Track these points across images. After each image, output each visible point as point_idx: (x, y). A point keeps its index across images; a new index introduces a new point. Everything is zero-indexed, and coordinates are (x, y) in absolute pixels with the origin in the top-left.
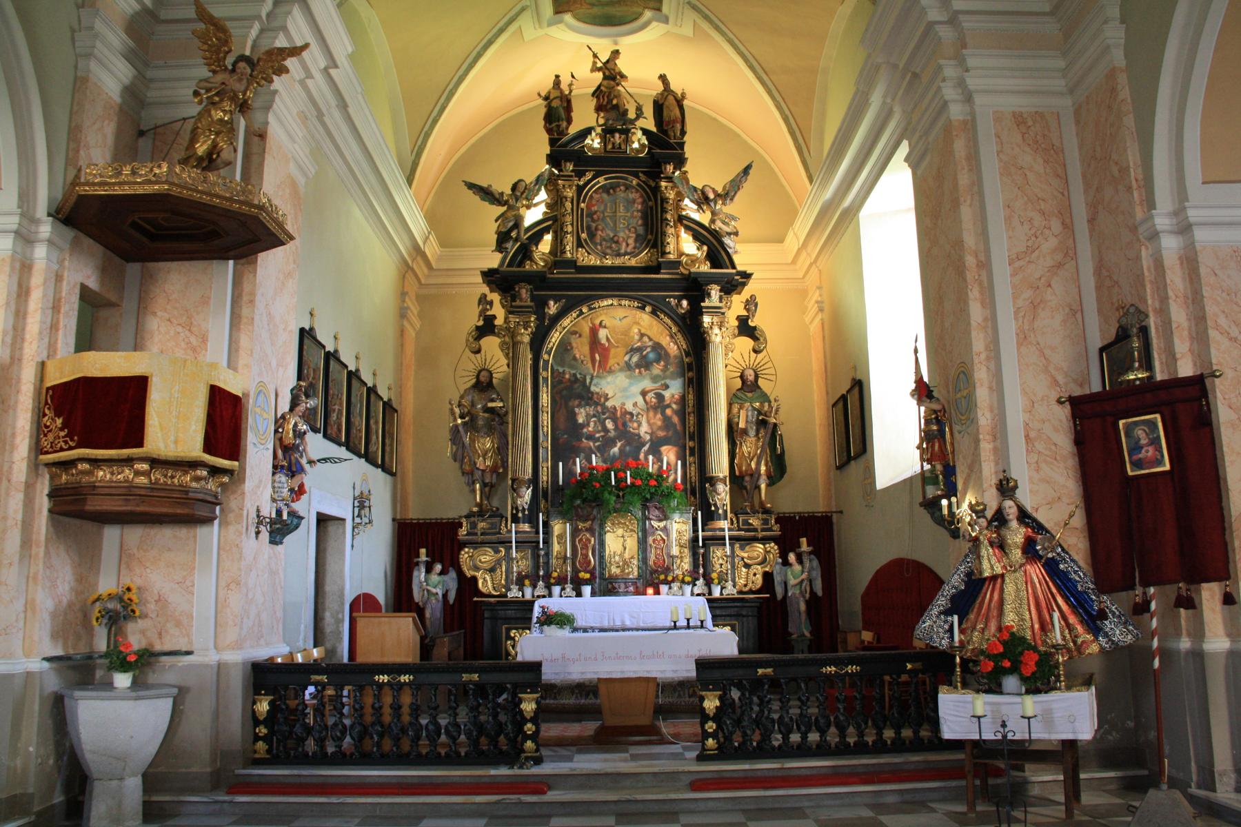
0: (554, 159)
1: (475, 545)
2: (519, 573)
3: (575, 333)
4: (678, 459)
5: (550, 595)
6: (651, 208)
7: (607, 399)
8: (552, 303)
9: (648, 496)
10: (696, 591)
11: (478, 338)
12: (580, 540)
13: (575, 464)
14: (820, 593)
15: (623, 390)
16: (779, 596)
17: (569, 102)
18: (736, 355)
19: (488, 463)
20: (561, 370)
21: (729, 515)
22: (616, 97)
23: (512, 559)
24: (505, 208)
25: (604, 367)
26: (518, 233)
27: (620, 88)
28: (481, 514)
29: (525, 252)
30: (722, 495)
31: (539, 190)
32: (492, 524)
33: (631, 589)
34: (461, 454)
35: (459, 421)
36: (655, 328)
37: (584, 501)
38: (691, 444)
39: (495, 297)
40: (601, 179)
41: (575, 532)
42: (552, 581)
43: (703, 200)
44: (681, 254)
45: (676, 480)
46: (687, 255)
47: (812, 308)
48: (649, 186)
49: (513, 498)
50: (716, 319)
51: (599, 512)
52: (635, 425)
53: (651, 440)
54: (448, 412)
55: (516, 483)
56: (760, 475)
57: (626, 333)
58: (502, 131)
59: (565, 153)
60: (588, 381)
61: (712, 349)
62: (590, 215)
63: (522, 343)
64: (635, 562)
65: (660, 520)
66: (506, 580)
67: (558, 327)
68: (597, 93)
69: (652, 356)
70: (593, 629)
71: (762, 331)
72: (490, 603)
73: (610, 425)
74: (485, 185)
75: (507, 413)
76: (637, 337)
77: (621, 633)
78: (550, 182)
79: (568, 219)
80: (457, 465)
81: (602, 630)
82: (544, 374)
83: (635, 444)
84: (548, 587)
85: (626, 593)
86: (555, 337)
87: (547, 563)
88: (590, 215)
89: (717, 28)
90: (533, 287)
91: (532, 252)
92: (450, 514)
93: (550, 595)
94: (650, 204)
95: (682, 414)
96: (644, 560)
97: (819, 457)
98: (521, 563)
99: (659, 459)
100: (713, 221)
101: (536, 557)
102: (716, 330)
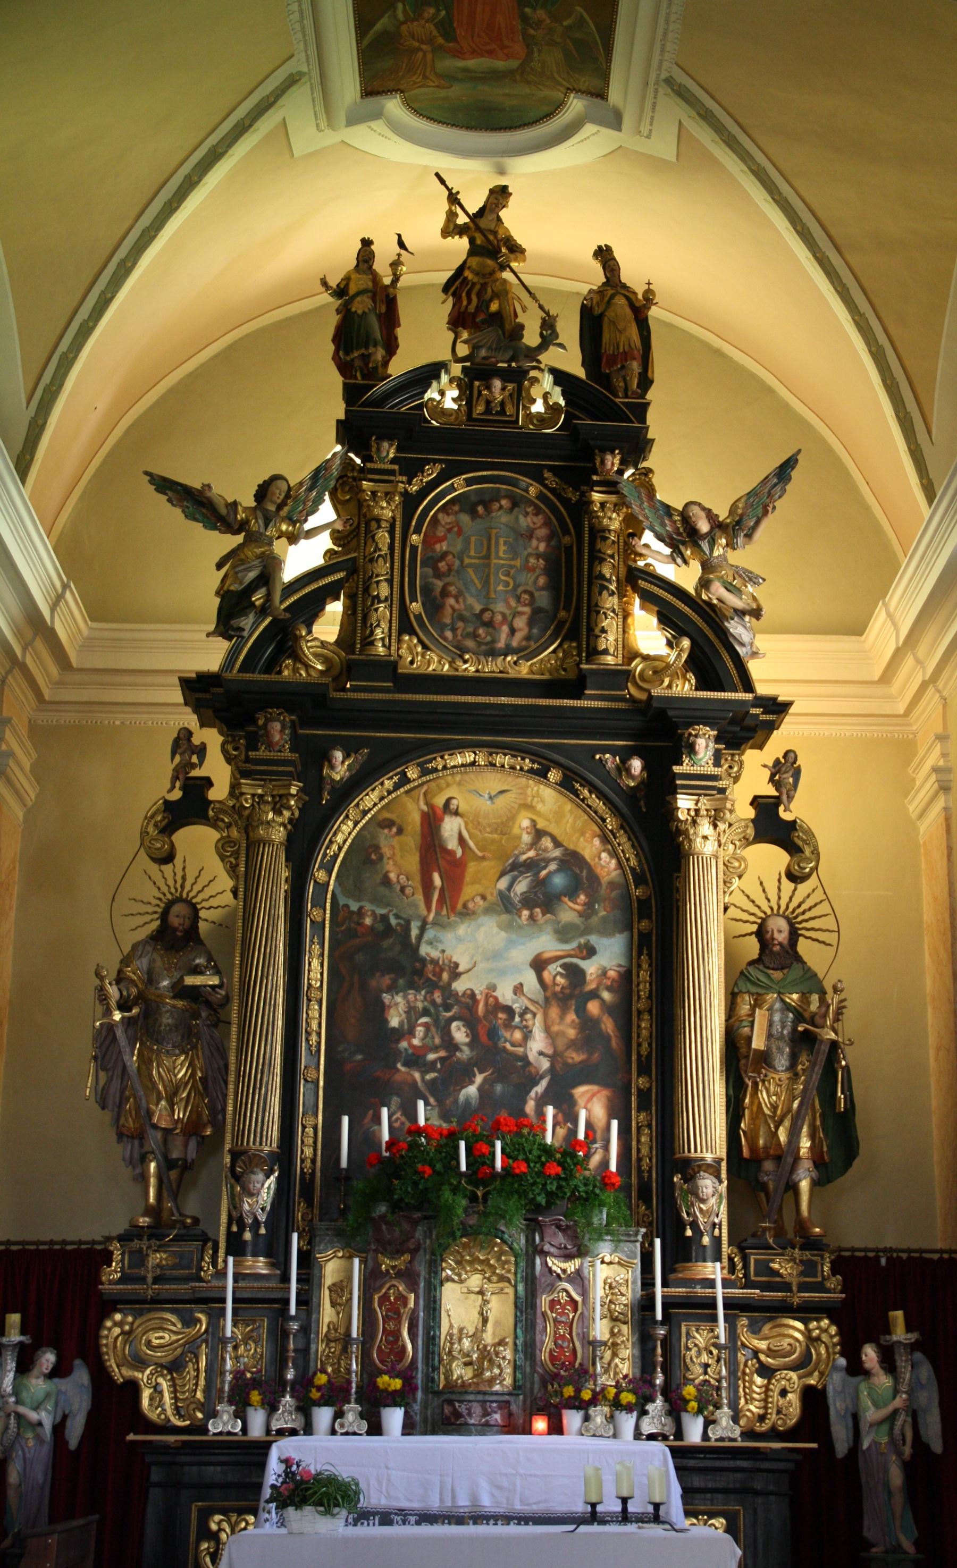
0: (351, 432)
1: (141, 1305)
2: (238, 1374)
3: (389, 824)
4: (611, 1116)
5: (308, 1429)
6: (569, 549)
7: (455, 974)
8: (338, 755)
9: (542, 1200)
10: (648, 1427)
11: (169, 829)
12: (384, 1299)
13: (378, 1120)
14: (937, 1446)
15: (492, 956)
16: (841, 1447)
17: (391, 303)
18: (749, 883)
19: (179, 1114)
20: (354, 906)
21: (726, 1249)
22: (495, 295)
23: (224, 1341)
24: (240, 539)
25: (452, 904)
26: (268, 597)
27: (507, 275)
28: (156, 1232)
29: (283, 639)
30: (712, 1201)
31: (319, 501)
32: (181, 1255)
33: (497, 1417)
34: (120, 1097)
35: (117, 1016)
37: (396, 1206)
39: (212, 738)
40: (458, 481)
41: (372, 1279)
43: (684, 535)
44: (632, 655)
45: (605, 1163)
46: (646, 658)
47: (926, 785)
48: (565, 502)
49: (232, 1197)
50: (705, 803)
51: (428, 1234)
52: (518, 1035)
53: (552, 1069)
54: (91, 994)
55: (243, 1163)
56: (797, 1158)
57: (504, 826)
58: (239, 360)
59: (377, 416)
60: (414, 932)
61: (694, 869)
62: (432, 561)
63: (268, 842)
65: (568, 1257)
66: (206, 1391)
67: (352, 812)
68: (456, 285)
70: (404, 1515)
71: (809, 832)
72: (166, 1447)
73: (460, 1034)
74: (195, 483)
75: (228, 999)
76: (526, 838)
77: (470, 1530)
78: (343, 484)
79: (382, 568)
80: (107, 1116)
81: (427, 1518)
82: (316, 914)
84: (305, 1409)
85: (485, 1428)
86: (344, 832)
87: (304, 1352)
88: (432, 561)
89: (731, 143)
90: (300, 719)
91: (297, 638)
92: (86, 1229)
93: (308, 1429)
94: (566, 540)
95: (624, 1012)
96: (529, 1349)
97: (934, 1119)
98: (244, 1352)
99: (568, 1114)
100: (704, 584)
101: (279, 1335)
102: (705, 827)
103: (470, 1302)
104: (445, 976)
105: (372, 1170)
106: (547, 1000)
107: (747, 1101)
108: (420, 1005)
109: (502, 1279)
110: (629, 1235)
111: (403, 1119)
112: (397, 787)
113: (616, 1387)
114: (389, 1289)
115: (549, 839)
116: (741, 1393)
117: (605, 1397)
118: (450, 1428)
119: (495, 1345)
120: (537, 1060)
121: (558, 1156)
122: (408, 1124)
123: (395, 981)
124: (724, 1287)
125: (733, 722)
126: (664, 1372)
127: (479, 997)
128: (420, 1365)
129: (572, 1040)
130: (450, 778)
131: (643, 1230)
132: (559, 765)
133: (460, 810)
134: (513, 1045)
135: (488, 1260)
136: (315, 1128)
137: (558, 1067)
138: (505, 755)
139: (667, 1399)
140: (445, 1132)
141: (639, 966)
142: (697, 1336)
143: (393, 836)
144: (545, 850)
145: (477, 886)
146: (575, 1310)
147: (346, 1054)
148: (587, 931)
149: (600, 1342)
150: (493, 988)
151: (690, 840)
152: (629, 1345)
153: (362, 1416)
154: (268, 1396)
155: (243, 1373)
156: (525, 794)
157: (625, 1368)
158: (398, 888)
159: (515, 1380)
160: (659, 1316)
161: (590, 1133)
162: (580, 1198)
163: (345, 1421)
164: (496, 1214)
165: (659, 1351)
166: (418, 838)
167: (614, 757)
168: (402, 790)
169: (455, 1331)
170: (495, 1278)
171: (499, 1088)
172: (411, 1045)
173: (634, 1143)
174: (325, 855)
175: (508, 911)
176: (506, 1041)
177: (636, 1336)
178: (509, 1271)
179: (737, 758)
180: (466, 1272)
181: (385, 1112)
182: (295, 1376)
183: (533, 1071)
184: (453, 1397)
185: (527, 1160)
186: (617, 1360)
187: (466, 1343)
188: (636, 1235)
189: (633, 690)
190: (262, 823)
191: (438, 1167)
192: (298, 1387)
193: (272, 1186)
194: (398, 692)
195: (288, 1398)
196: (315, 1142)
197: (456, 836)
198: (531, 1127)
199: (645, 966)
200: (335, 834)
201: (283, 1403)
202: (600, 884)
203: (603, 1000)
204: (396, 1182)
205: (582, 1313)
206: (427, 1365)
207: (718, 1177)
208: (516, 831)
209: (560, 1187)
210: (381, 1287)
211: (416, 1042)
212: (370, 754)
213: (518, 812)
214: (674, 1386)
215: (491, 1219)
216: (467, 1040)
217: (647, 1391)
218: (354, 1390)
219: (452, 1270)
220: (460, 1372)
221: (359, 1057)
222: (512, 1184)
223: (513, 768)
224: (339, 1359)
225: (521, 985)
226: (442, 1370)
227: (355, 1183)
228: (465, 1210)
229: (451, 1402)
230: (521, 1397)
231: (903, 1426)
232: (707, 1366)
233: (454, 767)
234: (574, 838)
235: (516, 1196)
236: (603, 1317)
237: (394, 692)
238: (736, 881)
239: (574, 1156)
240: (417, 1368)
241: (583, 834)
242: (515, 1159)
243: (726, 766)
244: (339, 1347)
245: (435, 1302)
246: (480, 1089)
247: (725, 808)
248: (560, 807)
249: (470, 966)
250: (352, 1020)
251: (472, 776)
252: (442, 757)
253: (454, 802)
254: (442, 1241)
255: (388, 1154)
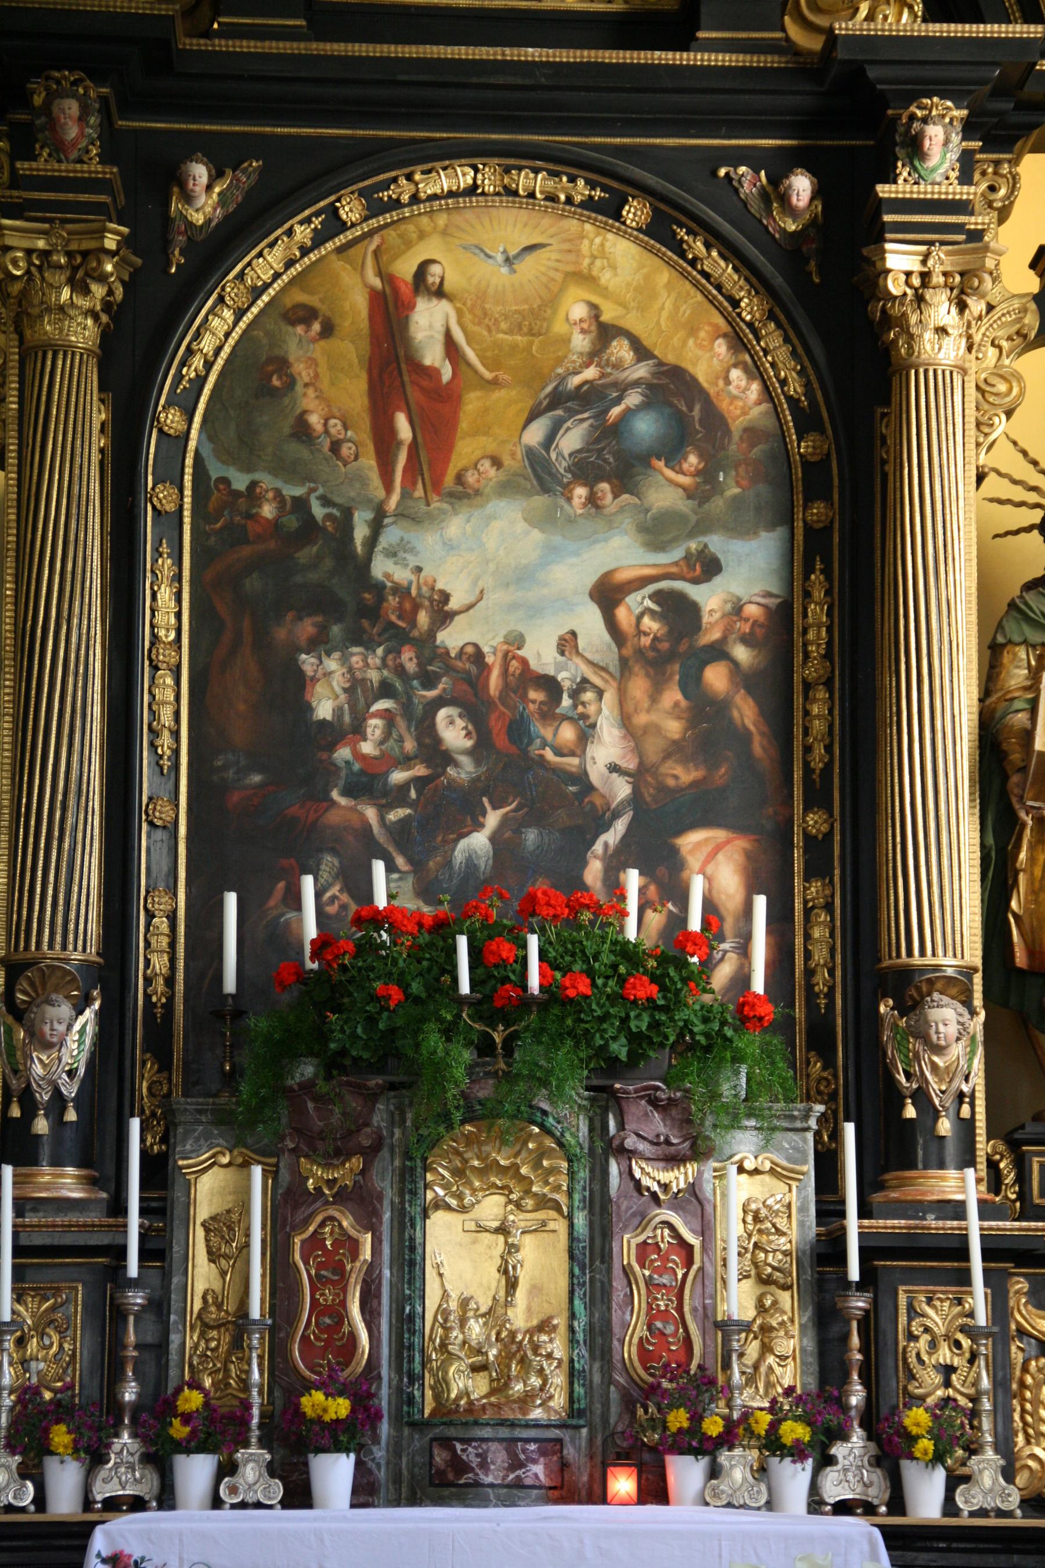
3: (305, 315)
4: (752, 888)
5: (167, 1498)
7: (443, 616)
8: (200, 172)
9: (620, 1049)
10: (836, 1487)
13: (295, 901)
15: (514, 577)
20: (240, 482)
21: (983, 1146)
25: (432, 473)
30: (954, 1048)
33: (538, 1470)
36: (666, 301)
37: (334, 1065)
38: (815, 822)
41: (288, 1206)
42: (179, 1430)
45: (743, 979)
50: (942, 260)
51: (397, 1118)
52: (567, 733)
53: (636, 799)
57: (534, 319)
60: (360, 533)
64: (558, 1347)
65: (673, 1160)
67: (231, 289)
69: (646, 427)
73: (453, 731)
76: (581, 342)
82: (164, 496)
83: (562, 817)
84: (159, 1459)
85: (514, 1492)
86: (215, 332)
87: (158, 1349)
93: (167, 1498)
95: (777, 687)
96: (598, 1339)
102: (941, 309)
103: (480, 1248)
104: (423, 618)
105: (286, 997)
106: (624, 662)
107: (1023, 856)
108: (374, 676)
109: (543, 1203)
110: (793, 1118)
111: (345, 898)
112: (319, 239)
113: (771, 1410)
114: (322, 1225)
115: (626, 343)
116: (1018, 1424)
117: (750, 1432)
118: (446, 1492)
119: (530, 1332)
120: (606, 781)
121: (652, 963)
122: (353, 907)
123: (323, 630)
124: (982, 1217)
125: (999, 91)
126: (866, 1382)
127: (489, 659)
128: (385, 1372)
129: (674, 742)
130: (425, 220)
131: (820, 1108)
132: (646, 191)
133: (447, 287)
134: (559, 752)
135: (515, 1167)
136: (172, 917)
137: (648, 794)
138: (536, 171)
139: (871, 1435)
140: (428, 922)
141: (807, 594)
142: (930, 1311)
143: (314, 341)
144: (618, 366)
145: (483, 440)
146: (689, 1262)
147: (231, 774)
148: (703, 526)
149: (738, 1323)
150: (519, 641)
151: (911, 336)
152: (795, 1330)
153: (272, 1470)
154: (87, 1434)
155: (36, 1391)
156: (578, 252)
157: (788, 1375)
158: (326, 444)
159: (571, 1400)
160: (854, 1273)
161: (714, 921)
162: (693, 1046)
163: (238, 1480)
164: (531, 1076)
165: (855, 1341)
166: (365, 345)
167: (757, 172)
168: (330, 246)
169: (453, 1305)
170: (529, 1203)
171: (531, 836)
172: (358, 755)
173: (799, 941)
174: (179, 377)
175: (545, 489)
176: (544, 744)
177: (809, 1313)
178: (557, 1188)
179: (1005, 169)
180: (474, 1191)
181: (308, 883)
182: (139, 1395)
183: (598, 802)
184: (452, 1432)
185: (590, 973)
186: (771, 1360)
187: (476, 1329)
188: (806, 1117)
189: (794, 32)
190: (49, 310)
191: (416, 987)
192: (144, 1416)
193: (90, 1029)
194: (319, 39)
195: (126, 1438)
196: (173, 945)
197: (440, 338)
198: (597, 909)
199: (818, 594)
200: (198, 336)
201: (116, 1447)
202: (727, 432)
203: (735, 663)
204: (334, 1017)
205: (701, 1269)
206: (399, 1370)
207: (968, 1003)
208: (559, 327)
209: (654, 1025)
210: (306, 1222)
211: (367, 748)
212: (262, 171)
213: (562, 289)
214: (884, 1411)
215: (522, 1086)
216: (469, 743)
217: (831, 1418)
218: (255, 1421)
219: (446, 1187)
220: (464, 1384)
221: (257, 778)
222: (562, 1019)
223: (552, 198)
224: (227, 1362)
225: (574, 634)
226: (428, 1380)
227: (252, 1022)
228: (470, 1070)
229: (446, 1443)
230: (584, 1431)
231: (84, 1026)
232: (948, 1370)
233: (434, 197)
234: (675, 341)
235: (569, 1042)
236: (744, 1276)
237: (306, 39)
238: (1001, 425)
239: (682, 964)
240: (379, 1377)
241: (693, 332)
242: (566, 971)
243: (984, 186)
244: (227, 1338)
245: (412, 1249)
246: (493, 839)
247: (982, 268)
248: (647, 277)
249: (472, 599)
250: (242, 707)
251: (469, 215)
252: (409, 177)
253: (435, 269)
254: (423, 1131)
255: (315, 966)
